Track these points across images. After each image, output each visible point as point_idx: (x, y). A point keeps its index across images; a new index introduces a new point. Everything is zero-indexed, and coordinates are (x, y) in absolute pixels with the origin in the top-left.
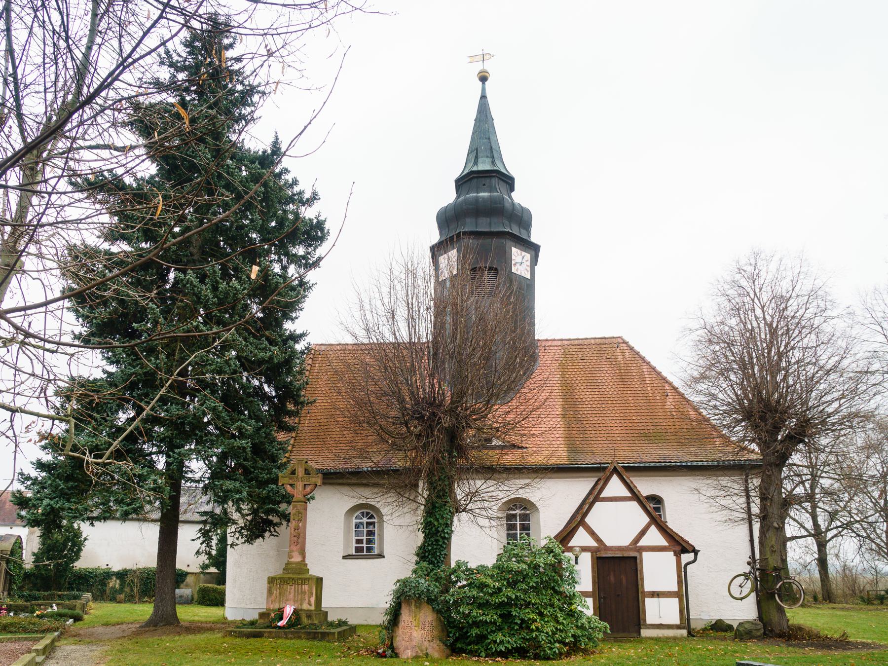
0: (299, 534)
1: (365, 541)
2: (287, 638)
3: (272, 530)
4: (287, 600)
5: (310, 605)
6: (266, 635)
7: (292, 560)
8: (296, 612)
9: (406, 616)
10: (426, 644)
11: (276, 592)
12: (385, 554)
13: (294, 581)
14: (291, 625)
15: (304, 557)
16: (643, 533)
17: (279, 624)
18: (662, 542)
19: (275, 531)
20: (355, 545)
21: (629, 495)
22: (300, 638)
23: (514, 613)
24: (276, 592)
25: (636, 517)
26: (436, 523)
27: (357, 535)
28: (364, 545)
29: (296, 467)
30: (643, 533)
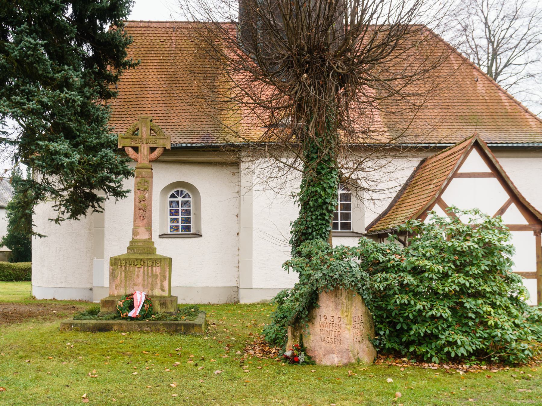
0: (146, 207)
1: (180, 221)
2: (141, 331)
3: (96, 205)
4: (134, 285)
5: (163, 290)
6: (115, 328)
7: (138, 237)
8: (148, 299)
9: (327, 308)
10: (357, 345)
11: (121, 275)
12: (203, 234)
13: (143, 262)
14: (146, 314)
15: (151, 235)
16: (502, 211)
17: (131, 314)
18: (522, 220)
19: (99, 206)
20: (170, 224)
21: (488, 170)
22: (157, 331)
23: (467, 305)
24: (121, 275)
25: (492, 195)
26: (322, 193)
27: (171, 214)
28: (180, 224)
29: (139, 126)
30: (502, 211)
